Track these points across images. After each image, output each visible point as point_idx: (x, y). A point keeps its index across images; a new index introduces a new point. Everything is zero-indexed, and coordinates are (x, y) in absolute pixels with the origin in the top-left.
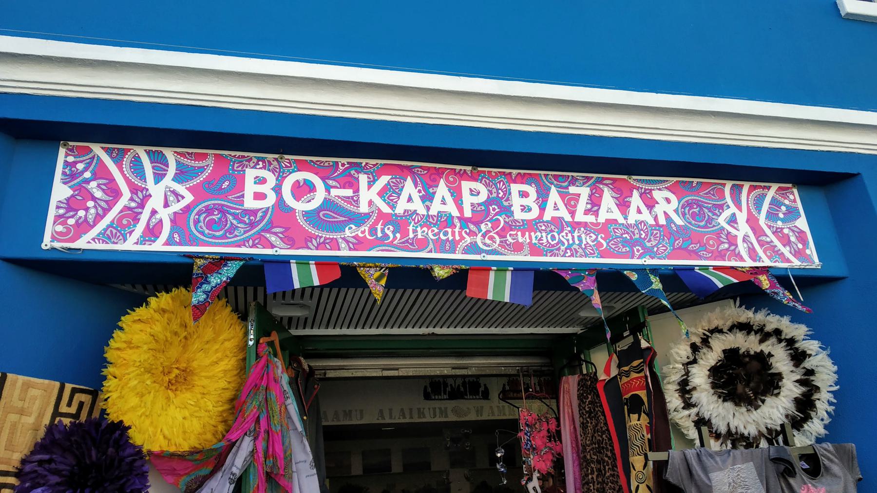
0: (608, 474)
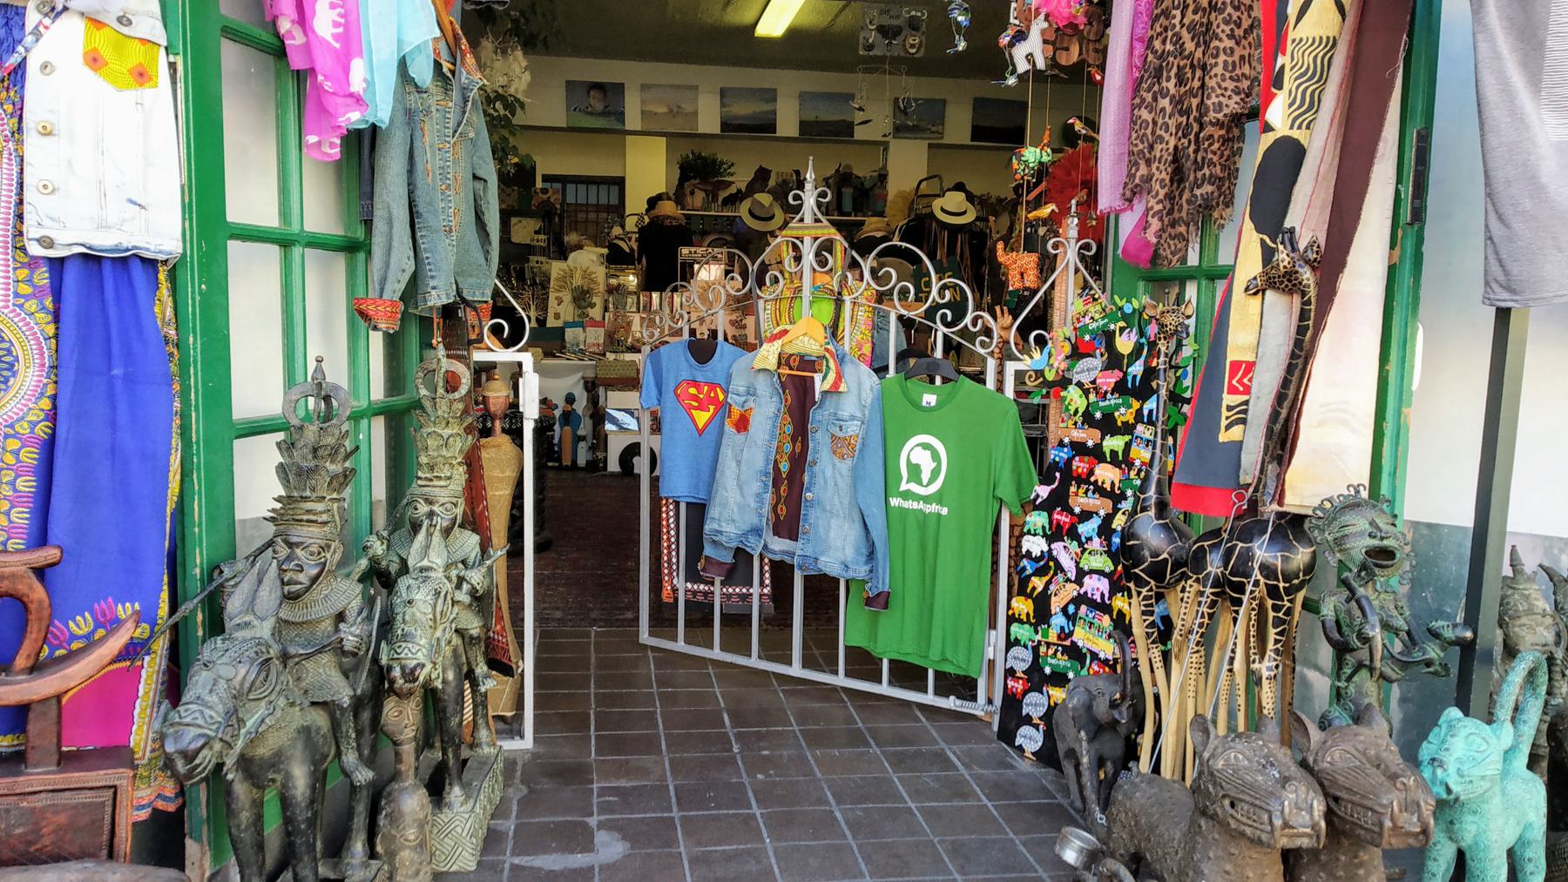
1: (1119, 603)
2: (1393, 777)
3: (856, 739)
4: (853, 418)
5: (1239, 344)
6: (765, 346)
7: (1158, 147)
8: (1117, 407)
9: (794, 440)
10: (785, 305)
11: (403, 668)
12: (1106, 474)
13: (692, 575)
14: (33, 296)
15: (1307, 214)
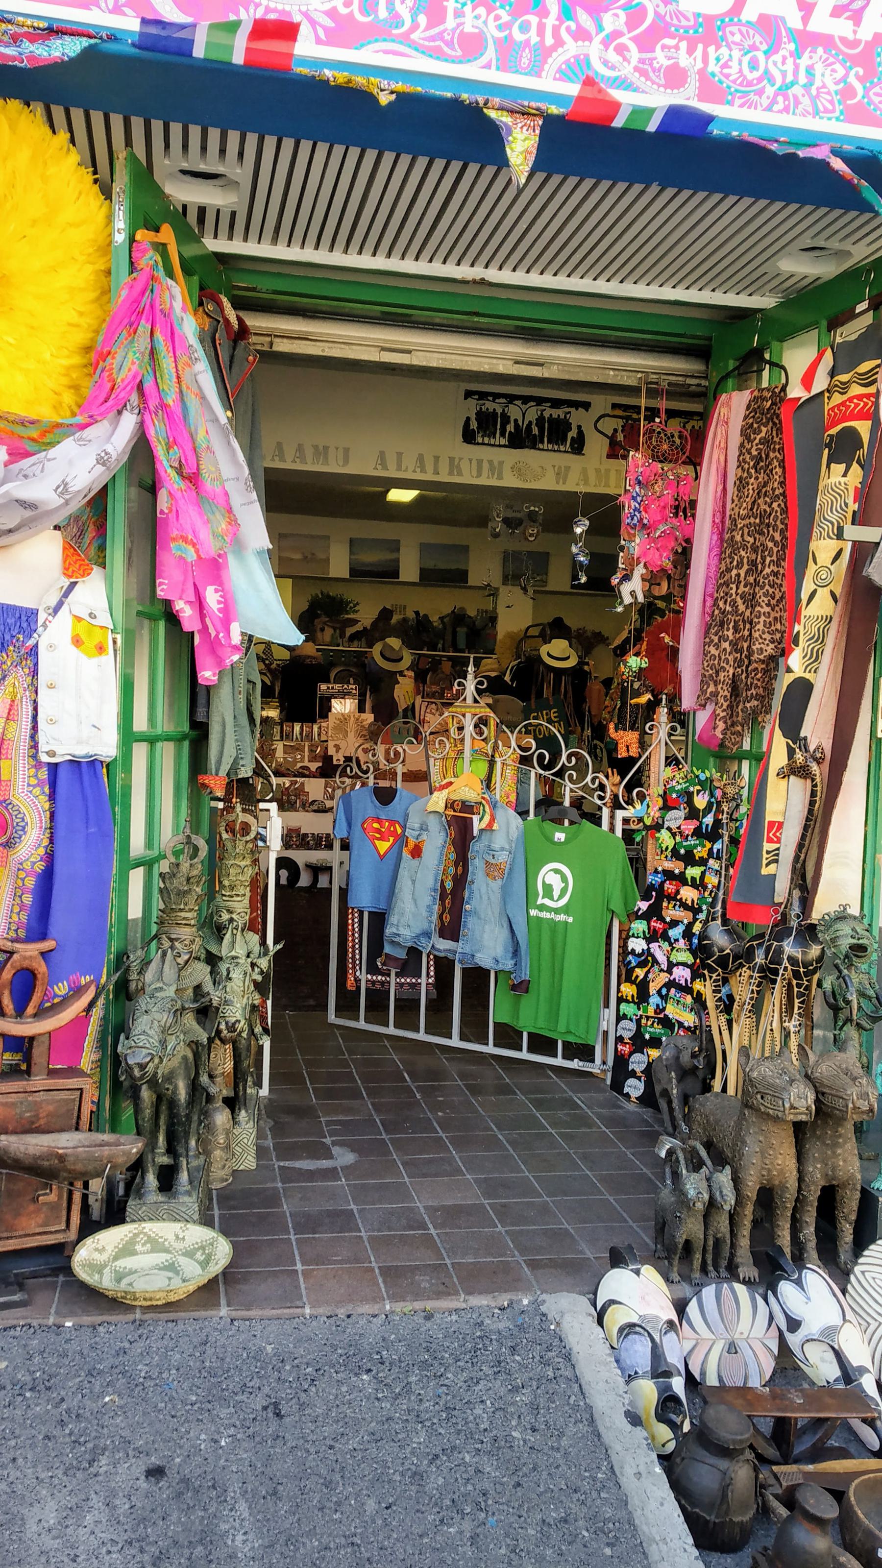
0: (767, 571)
1: (698, 986)
2: (854, 1079)
3: (504, 1090)
4: (503, 849)
5: (773, 810)
6: (436, 794)
7: (722, 674)
8: (696, 846)
9: (456, 865)
10: (450, 763)
11: (227, 1023)
12: (688, 894)
13: (372, 969)
14: (38, 785)
15: (818, 727)
